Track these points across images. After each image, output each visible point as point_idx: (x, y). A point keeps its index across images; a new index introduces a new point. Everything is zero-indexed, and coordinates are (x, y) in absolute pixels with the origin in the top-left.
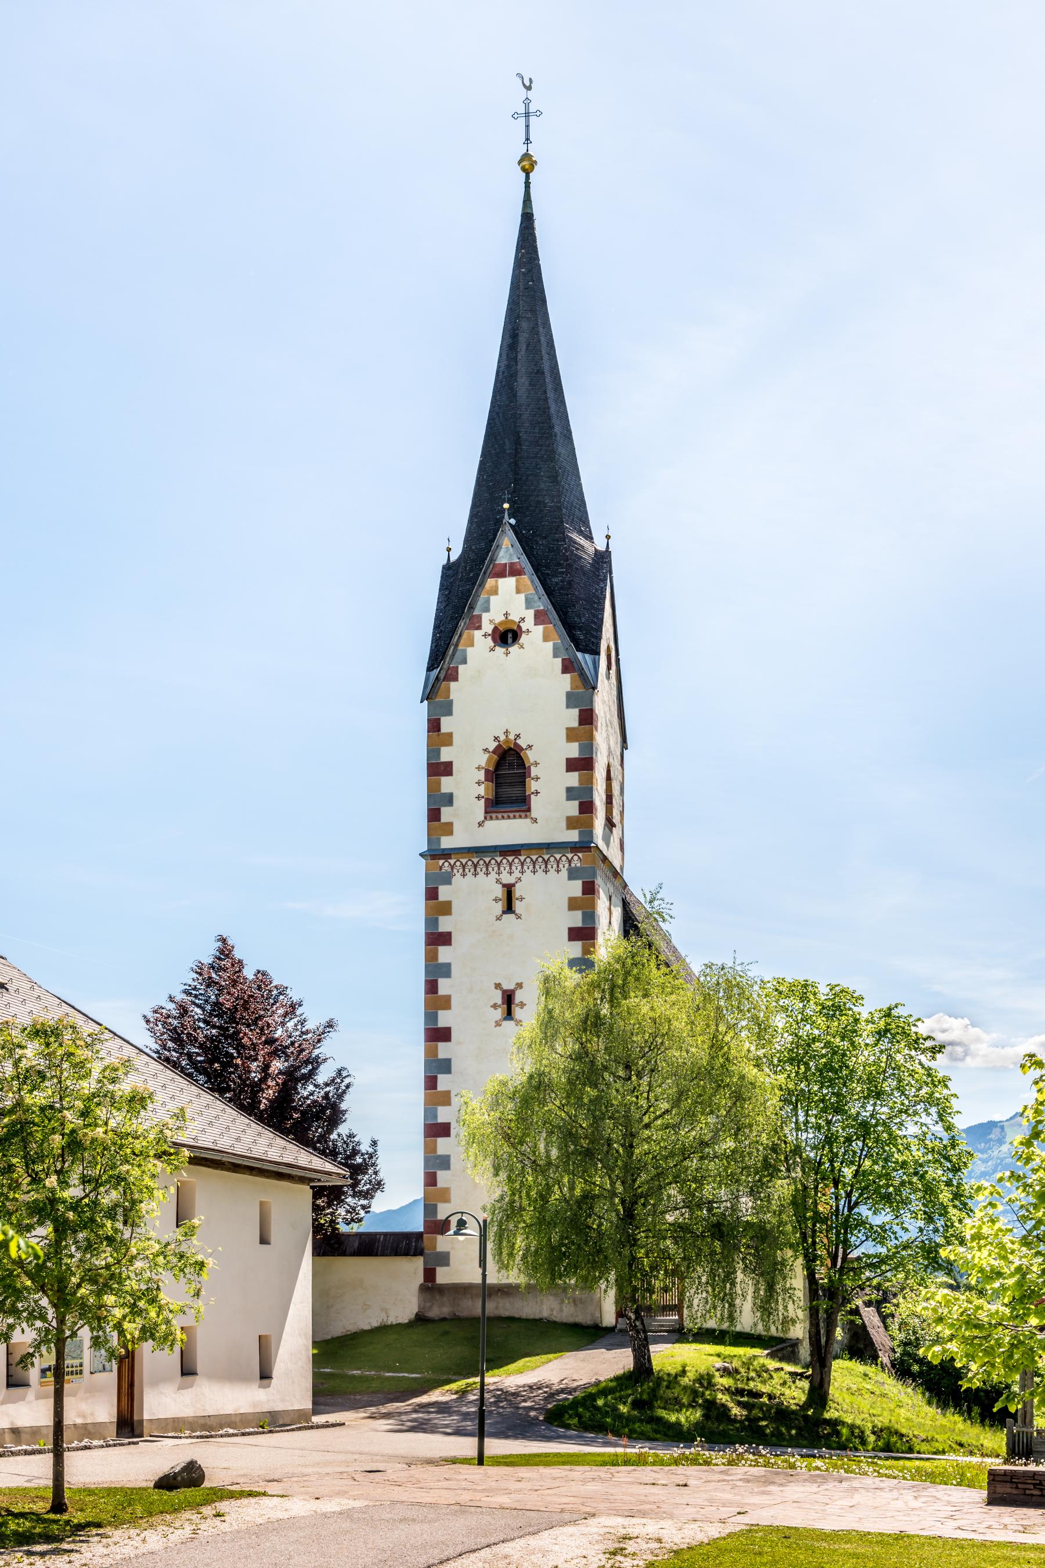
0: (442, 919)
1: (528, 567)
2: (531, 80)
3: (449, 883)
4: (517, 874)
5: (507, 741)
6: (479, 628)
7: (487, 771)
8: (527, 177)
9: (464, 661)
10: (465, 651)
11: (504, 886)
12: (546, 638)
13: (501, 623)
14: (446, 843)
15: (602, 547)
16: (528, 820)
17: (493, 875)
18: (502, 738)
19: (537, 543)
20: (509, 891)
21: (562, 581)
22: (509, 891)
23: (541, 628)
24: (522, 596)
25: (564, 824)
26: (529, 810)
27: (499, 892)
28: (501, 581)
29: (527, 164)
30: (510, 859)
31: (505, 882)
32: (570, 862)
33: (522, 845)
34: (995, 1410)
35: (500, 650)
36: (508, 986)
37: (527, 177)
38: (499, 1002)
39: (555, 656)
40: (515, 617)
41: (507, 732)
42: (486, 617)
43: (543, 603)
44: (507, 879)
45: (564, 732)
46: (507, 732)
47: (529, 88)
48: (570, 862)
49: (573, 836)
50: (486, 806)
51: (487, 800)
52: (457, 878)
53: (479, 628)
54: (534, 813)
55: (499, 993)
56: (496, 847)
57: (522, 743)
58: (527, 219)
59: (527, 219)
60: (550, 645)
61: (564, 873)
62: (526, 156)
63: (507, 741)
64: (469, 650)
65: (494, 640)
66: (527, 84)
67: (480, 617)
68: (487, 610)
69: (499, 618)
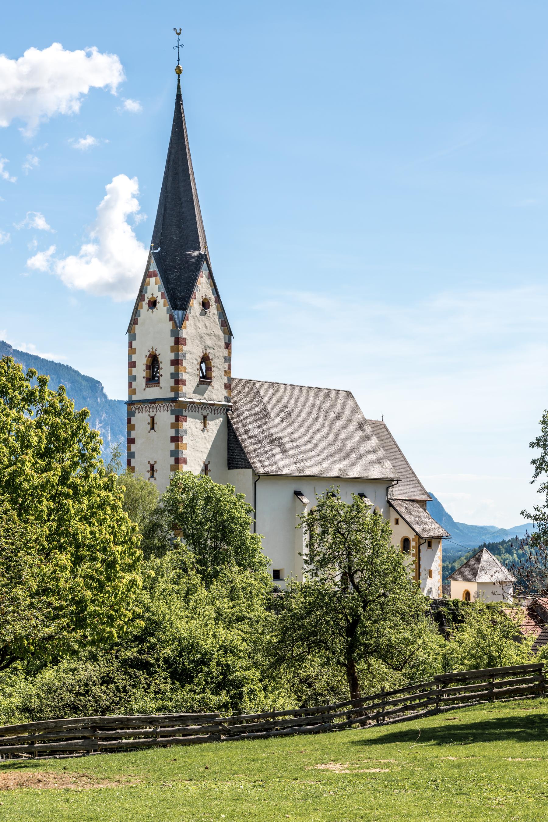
0: (133, 432)
1: (159, 274)
2: (180, 30)
3: (134, 416)
4: (155, 412)
5: (153, 352)
6: (144, 301)
7: (147, 365)
8: (179, 77)
9: (140, 316)
10: (140, 311)
11: (151, 417)
12: (164, 305)
13: (151, 298)
14: (135, 398)
15: (202, 252)
16: (159, 388)
17: (148, 413)
18: (151, 351)
19: (167, 258)
20: (153, 418)
21: (175, 276)
22: (153, 418)
23: (163, 300)
24: (157, 286)
25: (170, 390)
26: (159, 383)
27: (149, 420)
28: (151, 279)
29: (179, 71)
30: (153, 405)
31: (151, 416)
32: (171, 407)
33: (157, 399)
34: (494, 690)
35: (155, 310)
36: (152, 463)
37: (179, 77)
38: (149, 469)
39: (167, 313)
40: (155, 296)
41: (152, 348)
42: (146, 295)
43: (163, 290)
44: (152, 414)
45: (170, 348)
46: (152, 348)
47: (179, 34)
48: (171, 407)
49: (172, 395)
50: (146, 381)
51: (147, 378)
52: (137, 414)
53: (144, 301)
54: (161, 385)
55: (149, 465)
56: (149, 400)
57: (157, 353)
58: (179, 98)
59: (179, 98)
60: (166, 308)
61: (169, 412)
62: (178, 67)
63: (153, 352)
64: (141, 310)
65: (149, 306)
66: (178, 31)
67: (144, 295)
68: (146, 292)
69: (150, 296)
